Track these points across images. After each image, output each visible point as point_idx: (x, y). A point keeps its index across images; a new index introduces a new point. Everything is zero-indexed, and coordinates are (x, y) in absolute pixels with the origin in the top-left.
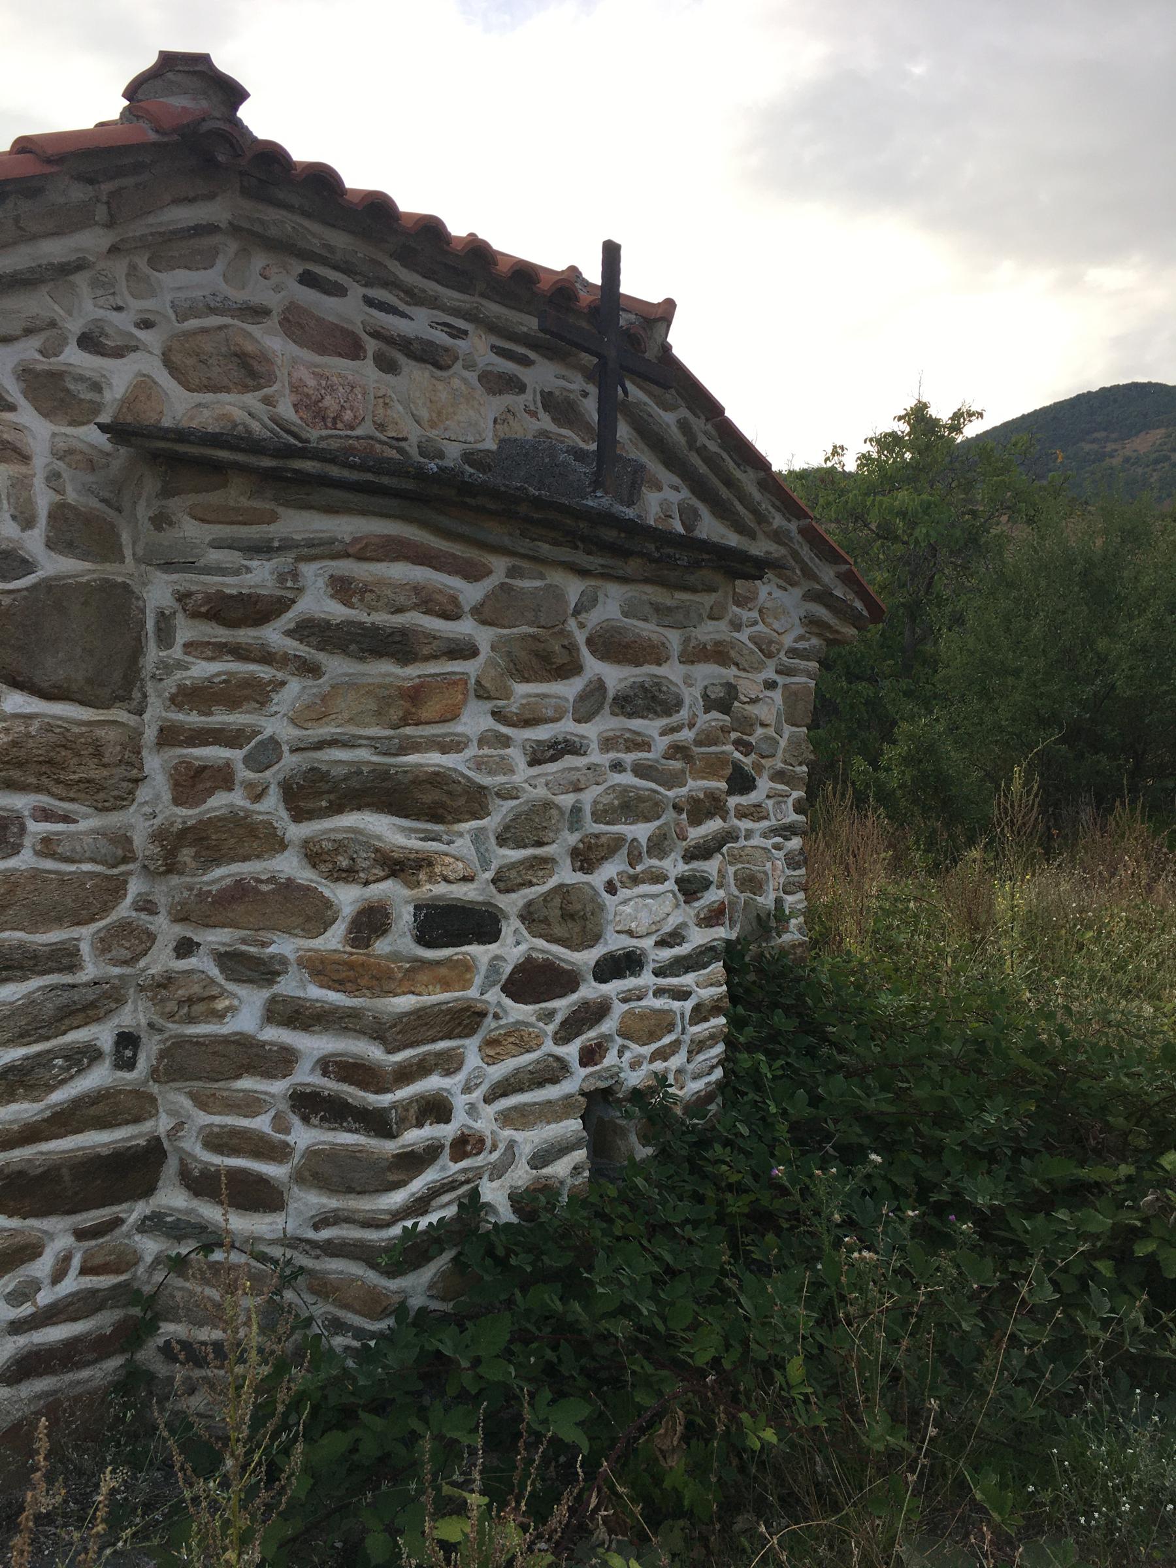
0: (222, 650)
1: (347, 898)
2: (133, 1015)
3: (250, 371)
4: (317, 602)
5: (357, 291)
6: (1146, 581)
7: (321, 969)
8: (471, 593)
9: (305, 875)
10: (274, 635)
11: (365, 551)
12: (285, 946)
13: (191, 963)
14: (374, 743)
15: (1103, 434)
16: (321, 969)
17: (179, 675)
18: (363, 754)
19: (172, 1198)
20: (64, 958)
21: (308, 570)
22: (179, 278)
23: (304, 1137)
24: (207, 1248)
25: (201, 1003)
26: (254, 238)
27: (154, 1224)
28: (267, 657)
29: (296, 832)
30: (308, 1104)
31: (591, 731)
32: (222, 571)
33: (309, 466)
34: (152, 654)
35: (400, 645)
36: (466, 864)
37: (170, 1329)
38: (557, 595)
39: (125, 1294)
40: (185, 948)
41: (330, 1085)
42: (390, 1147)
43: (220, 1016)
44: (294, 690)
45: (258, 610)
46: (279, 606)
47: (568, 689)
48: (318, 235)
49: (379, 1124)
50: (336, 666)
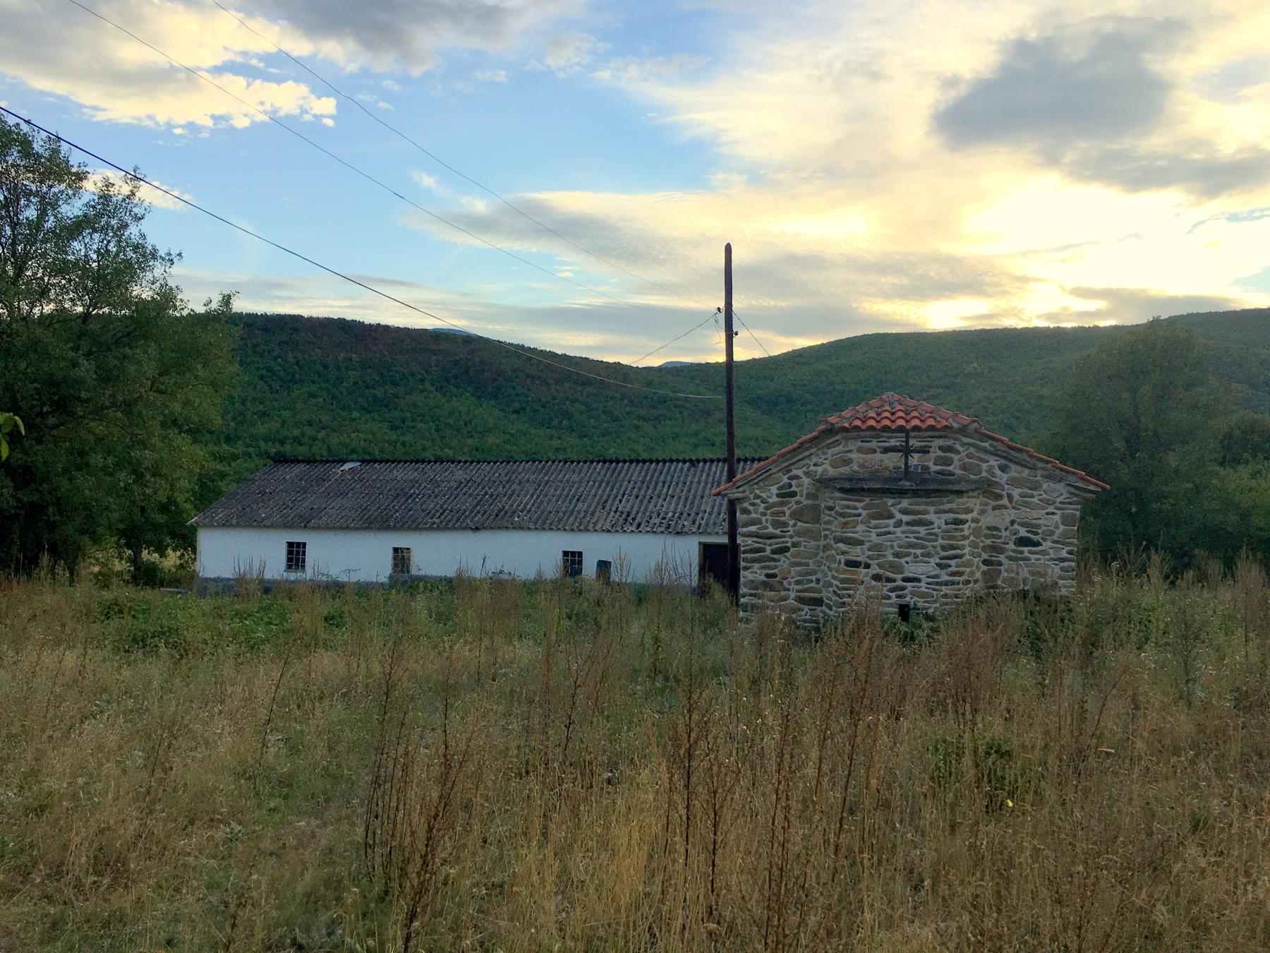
3: (848, 462)
20: (807, 565)
22: (831, 451)
26: (847, 439)
31: (898, 530)
36: (857, 553)
47: (891, 522)
48: (862, 434)
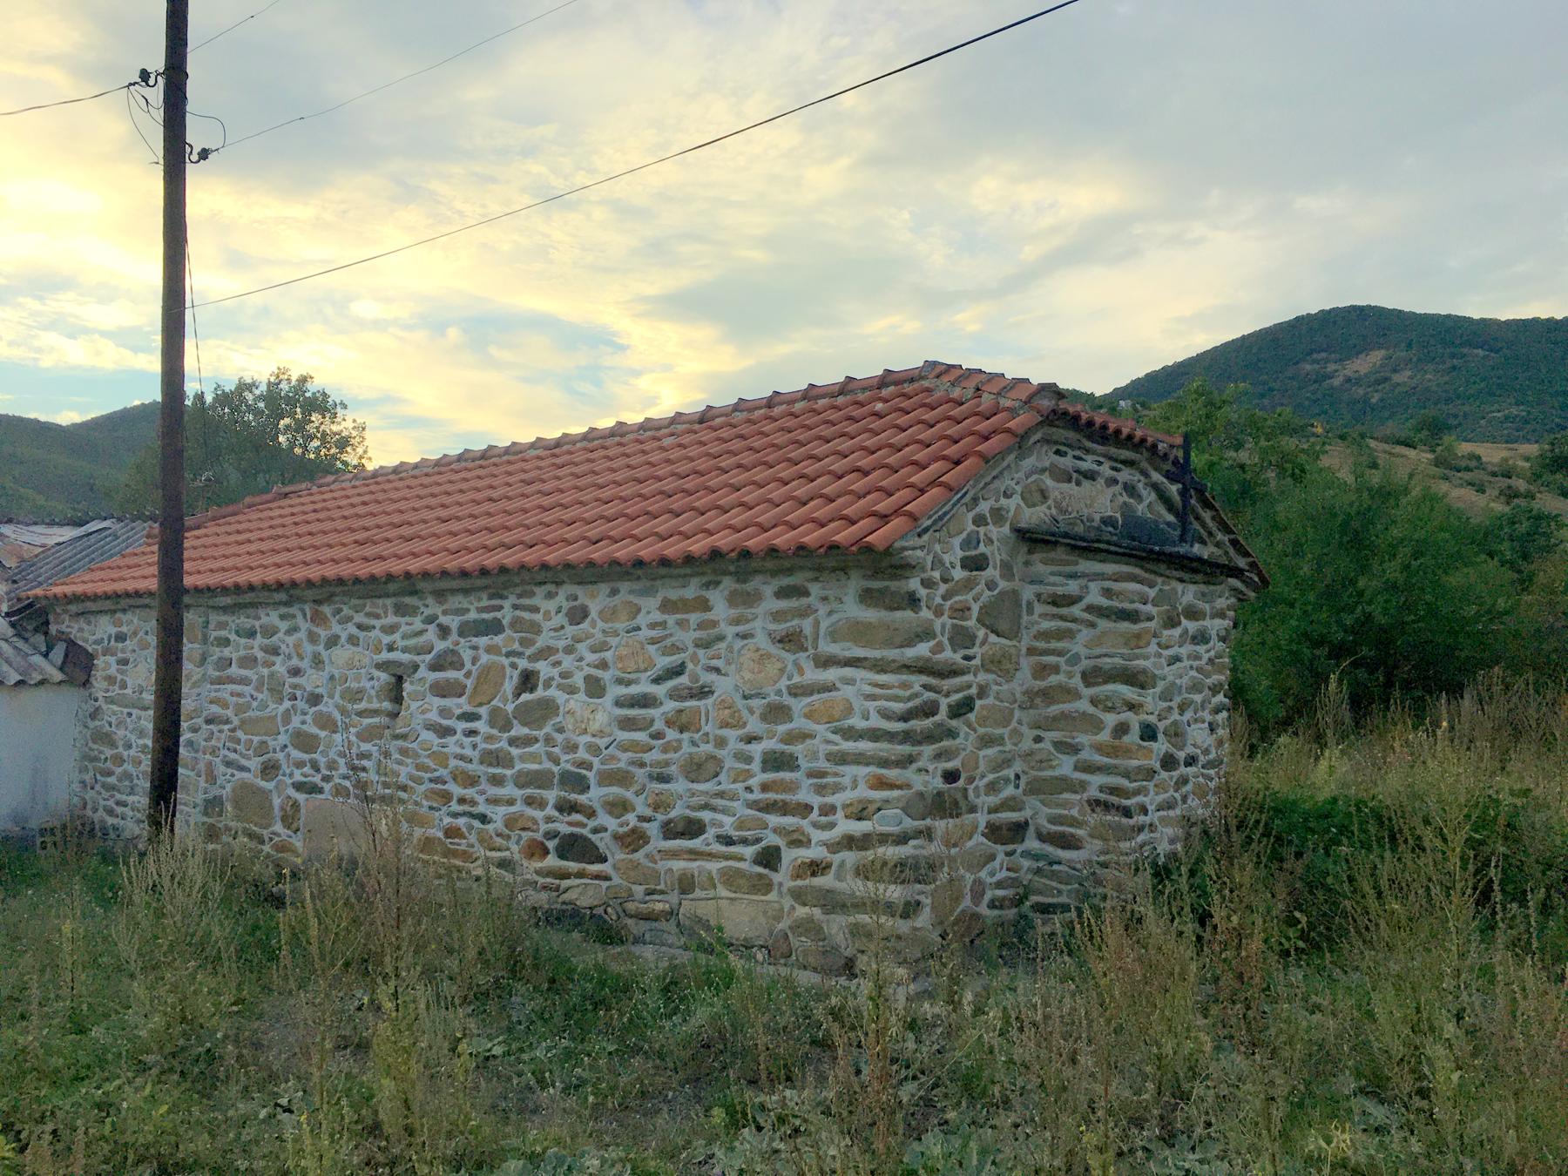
0: (1054, 617)
1: (1111, 719)
2: (1018, 766)
4: (1095, 597)
5: (1071, 453)
6: (1395, 532)
7: (1099, 748)
8: (1152, 593)
9: (1091, 710)
10: (1076, 610)
11: (1117, 578)
12: (1083, 739)
13: (1041, 745)
14: (1122, 656)
15: (1324, 355)
16: (1099, 748)
17: (1036, 627)
18: (1118, 661)
19: (1032, 843)
21: (1092, 585)
23: (1093, 819)
24: (1051, 864)
25: (1045, 763)
27: (1027, 854)
28: (1074, 620)
29: (1088, 692)
30: (1095, 804)
32: (1054, 584)
33: (1102, 546)
34: (1025, 618)
35: (1132, 616)
37: (1034, 899)
38: (1174, 589)
39: (1014, 883)
40: (1038, 739)
41: (1103, 797)
42: (1132, 822)
43: (1053, 768)
44: (1085, 634)
45: (1072, 600)
46: (1080, 598)
49: (1127, 813)
50: (1103, 624)
